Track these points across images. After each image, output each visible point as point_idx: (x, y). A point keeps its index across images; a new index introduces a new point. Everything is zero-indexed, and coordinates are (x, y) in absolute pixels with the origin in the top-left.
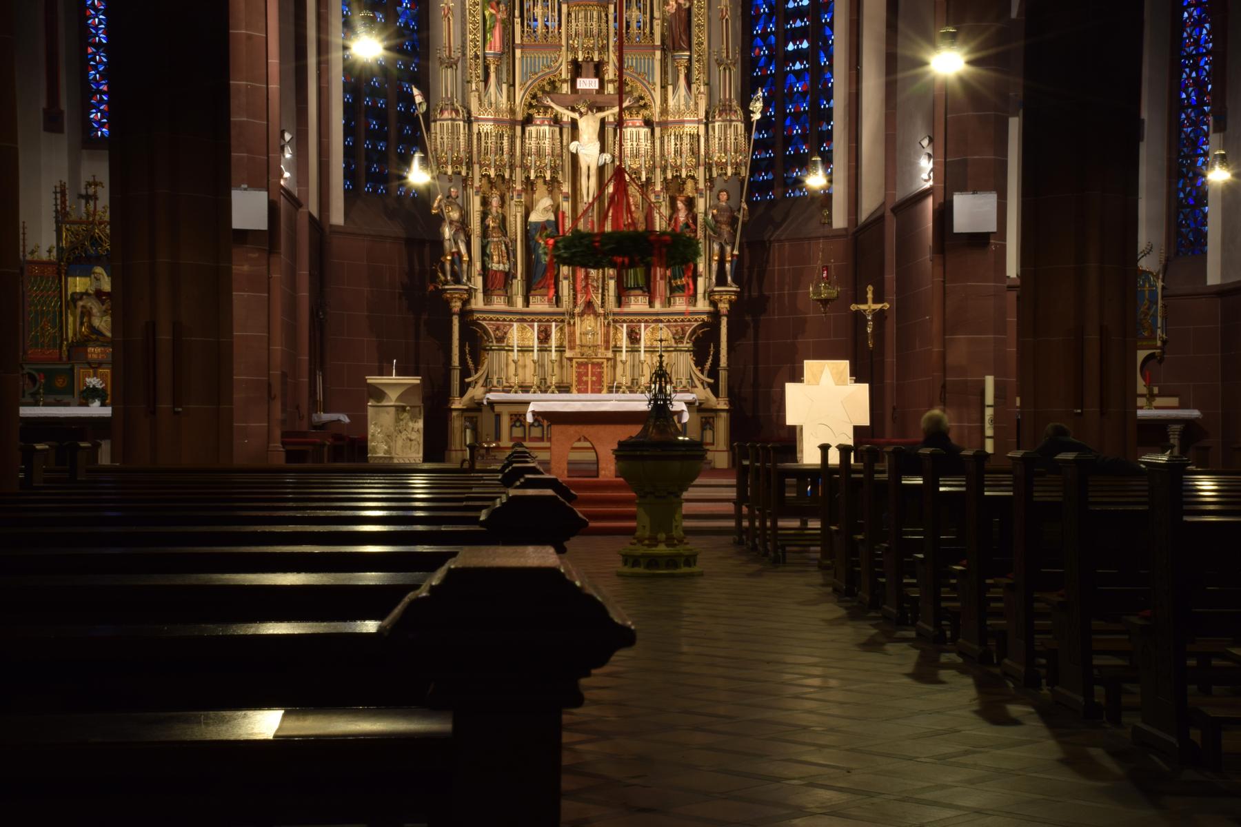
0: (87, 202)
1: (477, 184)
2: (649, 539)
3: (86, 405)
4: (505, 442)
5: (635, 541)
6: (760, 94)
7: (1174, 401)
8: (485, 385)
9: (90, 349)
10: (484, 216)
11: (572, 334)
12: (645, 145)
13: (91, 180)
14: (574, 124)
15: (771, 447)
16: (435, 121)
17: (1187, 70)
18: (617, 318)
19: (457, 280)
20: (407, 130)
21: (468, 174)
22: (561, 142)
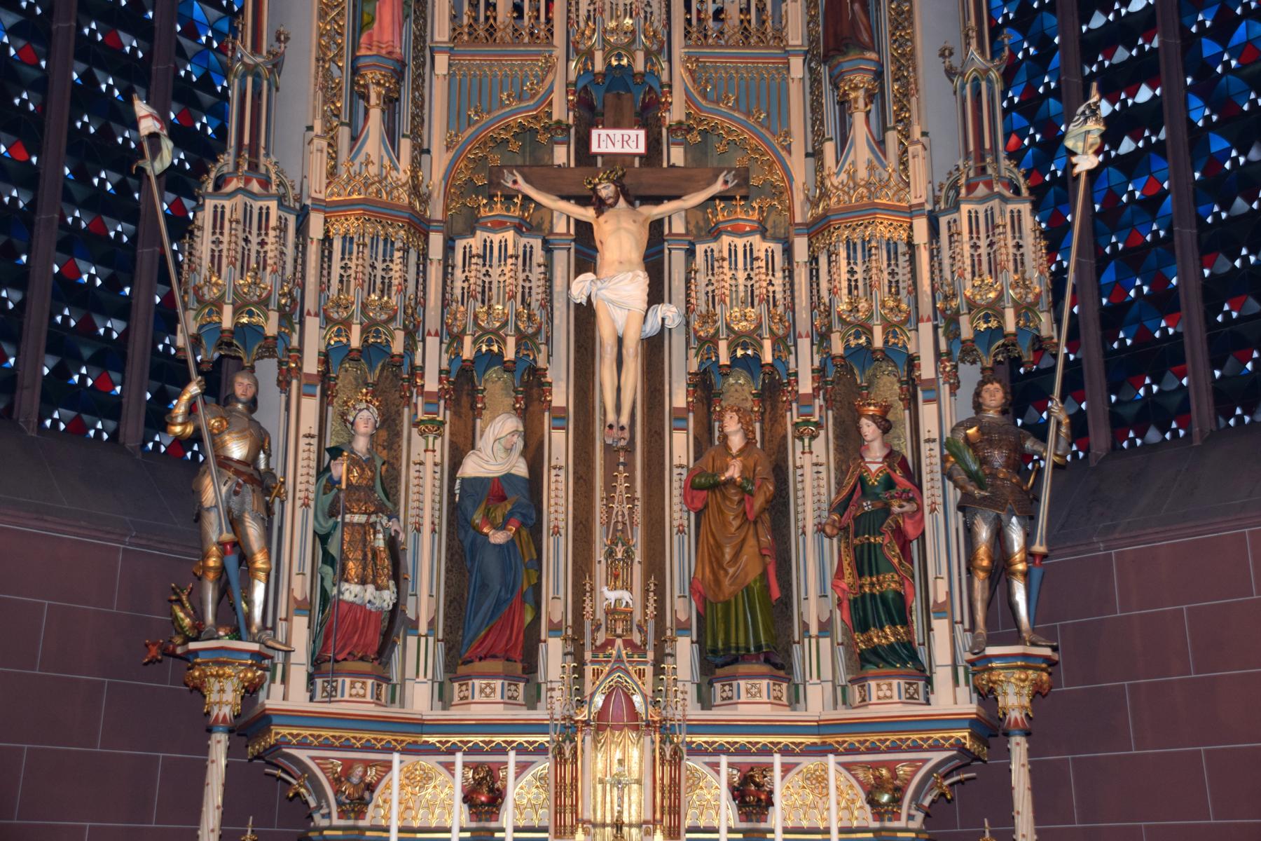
14: (584, 232)
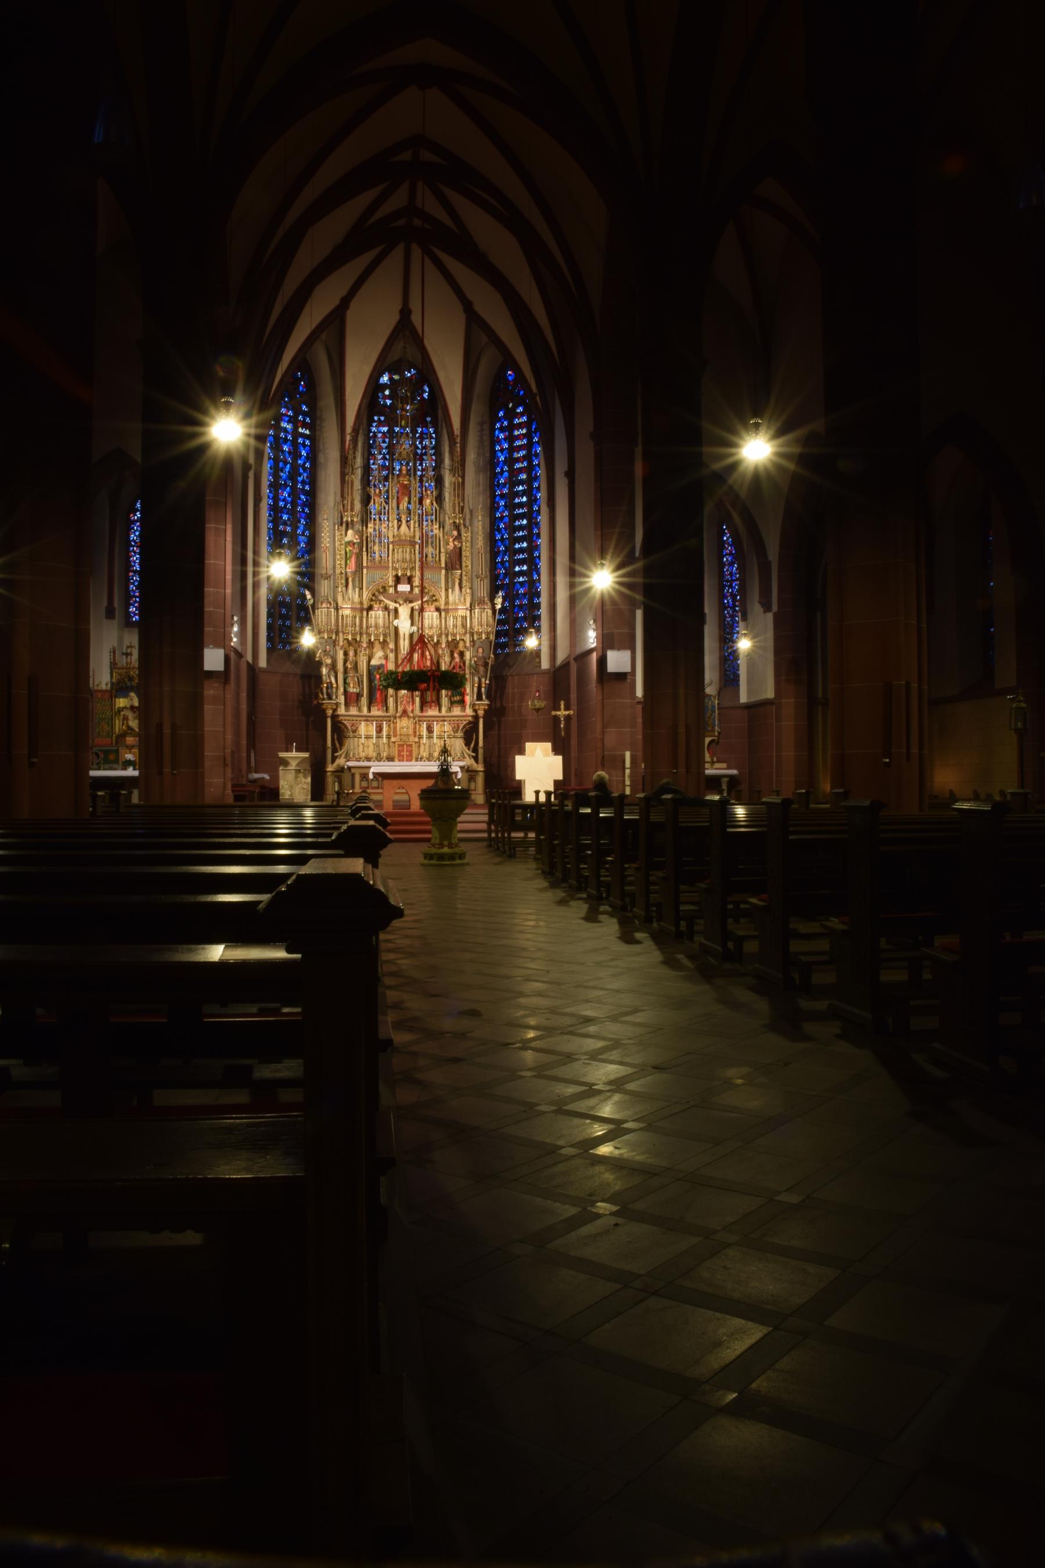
0: (127, 657)
1: (341, 643)
2: (438, 844)
3: (125, 769)
4: (357, 790)
5: (430, 846)
6: (500, 594)
7: (724, 765)
8: (346, 757)
9: (128, 739)
10: (345, 661)
11: (395, 728)
12: (436, 622)
13: (129, 645)
14: (396, 610)
15: (508, 792)
16: (318, 609)
17: (727, 588)
18: (420, 719)
19: (330, 698)
20: (302, 614)
21: (336, 638)
22: (389, 620)
